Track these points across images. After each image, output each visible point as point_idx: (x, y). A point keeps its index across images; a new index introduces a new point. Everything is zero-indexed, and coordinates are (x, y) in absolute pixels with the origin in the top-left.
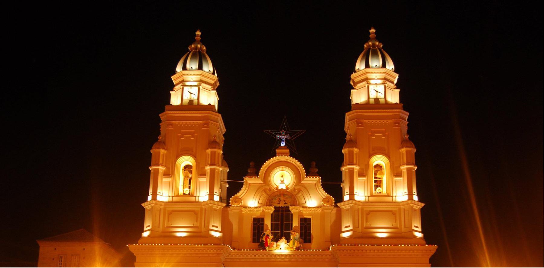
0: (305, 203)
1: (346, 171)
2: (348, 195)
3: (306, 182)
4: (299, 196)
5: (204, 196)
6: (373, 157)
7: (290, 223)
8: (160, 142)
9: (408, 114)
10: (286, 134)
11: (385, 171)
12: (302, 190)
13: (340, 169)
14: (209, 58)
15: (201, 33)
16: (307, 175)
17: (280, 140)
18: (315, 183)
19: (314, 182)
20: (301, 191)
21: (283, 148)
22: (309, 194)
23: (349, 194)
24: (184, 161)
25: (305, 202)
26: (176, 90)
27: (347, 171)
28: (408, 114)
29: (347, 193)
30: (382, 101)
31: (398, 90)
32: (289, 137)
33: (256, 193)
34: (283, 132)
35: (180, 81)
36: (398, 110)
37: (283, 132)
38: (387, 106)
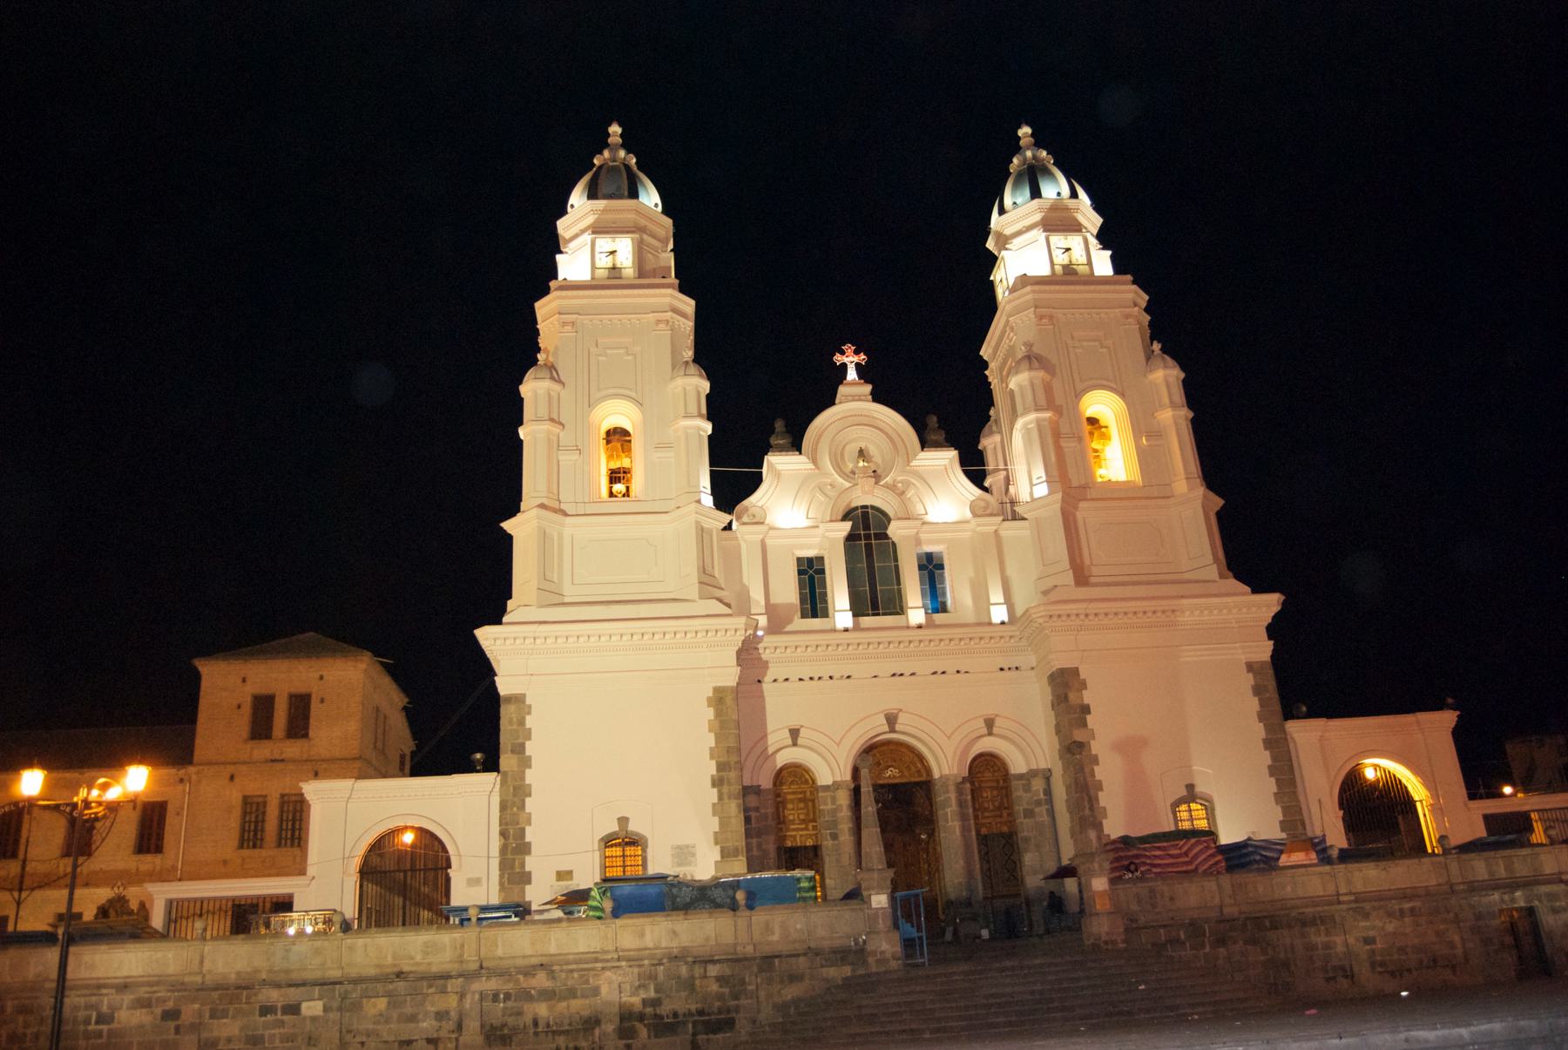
0: (926, 514)
1: (1029, 426)
2: (1045, 483)
3: (927, 464)
4: (909, 498)
5: (694, 601)
6: (1095, 391)
7: (890, 566)
8: (541, 366)
9: (1147, 298)
10: (856, 352)
11: (1113, 431)
12: (913, 484)
13: (978, 442)
14: (646, 178)
15: (623, 130)
16: (923, 448)
17: (844, 366)
18: (945, 466)
19: (942, 463)
20: (912, 485)
21: (853, 383)
22: (931, 489)
23: (1047, 481)
24: (613, 414)
25: (924, 512)
26: (570, 253)
27: (1033, 425)
28: (1147, 298)
29: (1038, 478)
30: (1083, 269)
31: (1109, 253)
32: (864, 359)
33: (797, 499)
34: (849, 348)
35: (582, 228)
36: (440, 876)
37: (849, 348)
38: (1092, 280)
